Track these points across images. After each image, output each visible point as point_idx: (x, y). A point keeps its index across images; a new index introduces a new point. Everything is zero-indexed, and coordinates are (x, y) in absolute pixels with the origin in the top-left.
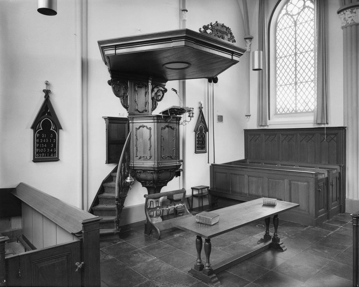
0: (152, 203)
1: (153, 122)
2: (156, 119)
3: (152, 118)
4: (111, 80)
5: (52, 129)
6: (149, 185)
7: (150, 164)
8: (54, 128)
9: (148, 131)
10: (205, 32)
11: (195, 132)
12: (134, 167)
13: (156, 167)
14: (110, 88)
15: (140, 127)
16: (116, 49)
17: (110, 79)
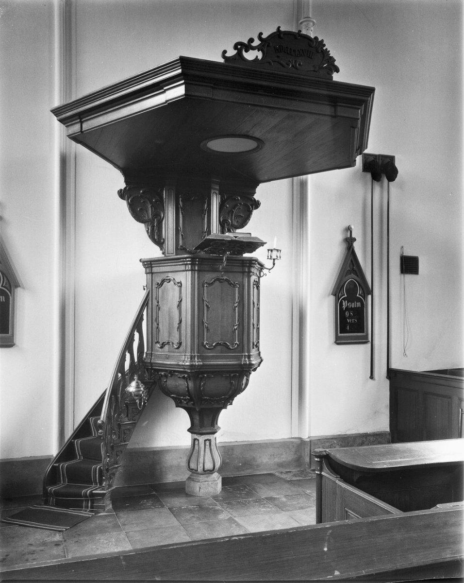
0: (208, 443)
1: (183, 271)
2: (188, 263)
3: (181, 262)
4: (125, 188)
5: (344, 295)
6: (187, 403)
7: (184, 360)
8: (6, 284)
9: (177, 288)
10: (239, 54)
11: (335, 295)
12: (151, 363)
13: (187, 366)
14: (124, 204)
15: (163, 281)
16: (82, 123)
17: (122, 185)
